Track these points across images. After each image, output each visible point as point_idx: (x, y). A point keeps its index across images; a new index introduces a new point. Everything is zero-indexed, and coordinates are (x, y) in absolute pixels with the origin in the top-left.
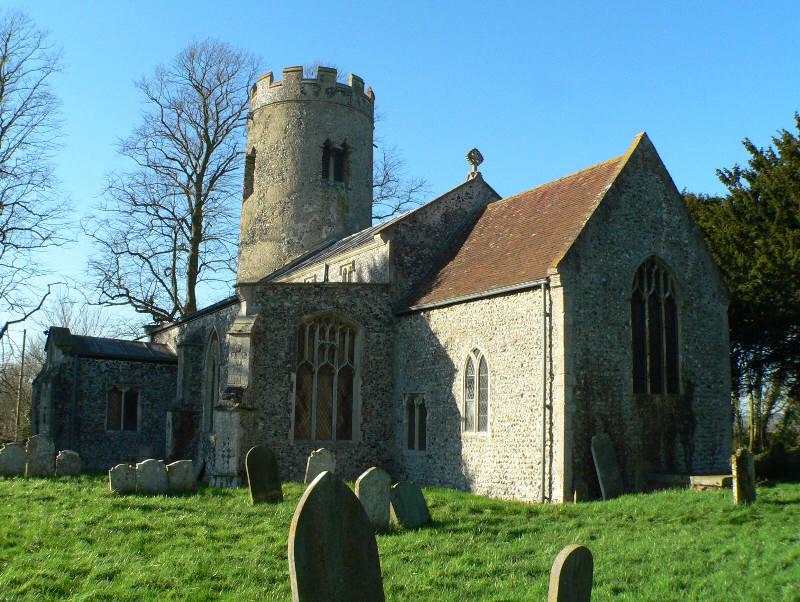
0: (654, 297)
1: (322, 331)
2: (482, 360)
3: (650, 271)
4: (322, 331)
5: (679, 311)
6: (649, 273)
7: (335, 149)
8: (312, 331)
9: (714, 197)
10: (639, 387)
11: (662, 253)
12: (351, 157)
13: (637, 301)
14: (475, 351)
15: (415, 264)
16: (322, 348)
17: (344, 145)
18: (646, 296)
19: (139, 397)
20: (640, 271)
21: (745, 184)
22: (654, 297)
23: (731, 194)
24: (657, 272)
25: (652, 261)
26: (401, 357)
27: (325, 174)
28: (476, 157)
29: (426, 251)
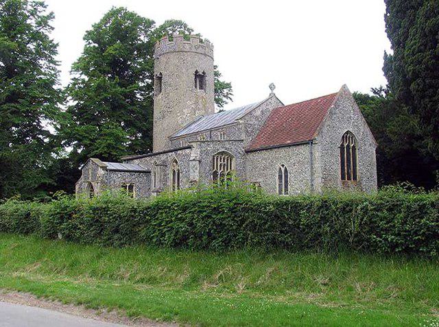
0: (348, 146)
1: (221, 159)
2: (286, 169)
3: (348, 136)
4: (221, 159)
5: (357, 150)
6: (346, 137)
7: (200, 75)
8: (217, 159)
9: (103, 16)
10: (343, 178)
11: (351, 130)
12: (207, 78)
13: (342, 147)
14: (283, 166)
15: (253, 132)
16: (221, 165)
17: (204, 73)
18: (345, 145)
19: (134, 187)
20: (343, 137)
21: (383, 94)
22: (348, 146)
23: (157, 25)
24: (349, 137)
25: (347, 132)
26: (249, 168)
27: (196, 87)
28: (272, 87)
29: (256, 126)
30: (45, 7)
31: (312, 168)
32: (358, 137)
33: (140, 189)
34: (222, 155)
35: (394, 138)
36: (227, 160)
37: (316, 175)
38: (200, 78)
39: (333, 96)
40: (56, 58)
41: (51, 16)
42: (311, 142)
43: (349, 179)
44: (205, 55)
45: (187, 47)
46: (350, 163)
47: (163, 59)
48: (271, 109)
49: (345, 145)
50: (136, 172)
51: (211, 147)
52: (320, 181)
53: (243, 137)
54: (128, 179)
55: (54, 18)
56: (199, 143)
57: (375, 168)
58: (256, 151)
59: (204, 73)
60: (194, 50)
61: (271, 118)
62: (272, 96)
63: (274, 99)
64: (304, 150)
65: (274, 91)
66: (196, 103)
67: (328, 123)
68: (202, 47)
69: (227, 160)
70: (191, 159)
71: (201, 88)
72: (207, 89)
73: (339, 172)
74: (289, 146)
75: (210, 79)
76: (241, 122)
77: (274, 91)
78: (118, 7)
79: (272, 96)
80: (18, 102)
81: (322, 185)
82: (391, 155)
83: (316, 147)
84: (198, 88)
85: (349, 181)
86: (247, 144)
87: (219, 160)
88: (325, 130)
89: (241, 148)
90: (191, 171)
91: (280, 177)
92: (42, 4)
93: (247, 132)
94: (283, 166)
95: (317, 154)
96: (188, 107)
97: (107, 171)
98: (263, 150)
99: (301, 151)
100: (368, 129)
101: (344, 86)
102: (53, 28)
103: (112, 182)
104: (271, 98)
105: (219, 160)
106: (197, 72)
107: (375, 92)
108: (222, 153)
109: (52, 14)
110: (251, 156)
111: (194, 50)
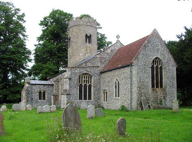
0: (157, 67)
5: (163, 69)
6: (156, 61)
8: (82, 77)
10: (153, 86)
11: (159, 57)
13: (152, 68)
16: (84, 81)
17: (90, 35)
18: (155, 66)
20: (153, 61)
22: (157, 67)
25: (156, 58)
28: (118, 37)
30: (20, 11)
31: (131, 81)
32: (164, 61)
33: (49, 94)
34: (85, 75)
35: (188, 61)
36: (89, 78)
37: (134, 85)
38: (88, 38)
39: (147, 37)
40: (26, 34)
41: (23, 15)
42: (130, 65)
43: (157, 87)
44: (91, 26)
45: (82, 22)
46: (158, 77)
47: (71, 30)
48: (117, 49)
49: (155, 66)
50: (46, 85)
51: (77, 71)
52: (136, 89)
53: (99, 65)
54: (42, 89)
55: (25, 16)
56: (70, 68)
57: (176, 80)
58: (105, 72)
59: (90, 35)
60: (85, 24)
61: (116, 54)
62: (118, 42)
63: (119, 44)
64: (127, 70)
65: (119, 39)
66: (86, 50)
67: (142, 52)
68: (89, 22)
69: (89, 78)
70: (65, 77)
71: (89, 43)
72: (92, 43)
73: (150, 83)
74: (120, 68)
75: (94, 39)
76: (98, 56)
77: (119, 39)
78: (56, 9)
79: (118, 42)
80: (5, 54)
81: (137, 91)
82: (187, 72)
83: (134, 67)
84: (88, 42)
85: (157, 89)
86: (102, 67)
87: (83, 78)
88: (140, 56)
89: (97, 71)
90: (65, 84)
91: (116, 87)
92: (18, 10)
93: (102, 61)
94: (117, 80)
95: (134, 72)
96: (82, 53)
97: (30, 84)
98: (108, 71)
99: (126, 71)
100: (171, 56)
101: (155, 30)
102: (25, 21)
103: (34, 90)
104: (117, 43)
105: (83, 78)
106: (86, 35)
107: (178, 37)
108: (85, 74)
109: (24, 14)
110: (103, 74)
111: (85, 24)
